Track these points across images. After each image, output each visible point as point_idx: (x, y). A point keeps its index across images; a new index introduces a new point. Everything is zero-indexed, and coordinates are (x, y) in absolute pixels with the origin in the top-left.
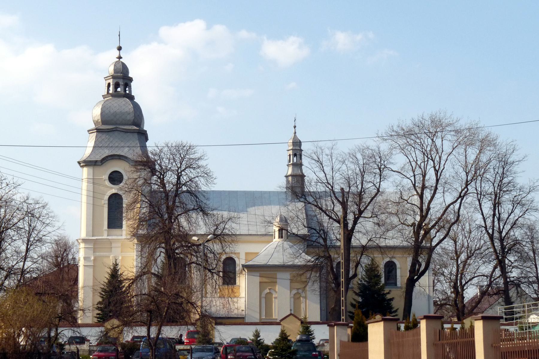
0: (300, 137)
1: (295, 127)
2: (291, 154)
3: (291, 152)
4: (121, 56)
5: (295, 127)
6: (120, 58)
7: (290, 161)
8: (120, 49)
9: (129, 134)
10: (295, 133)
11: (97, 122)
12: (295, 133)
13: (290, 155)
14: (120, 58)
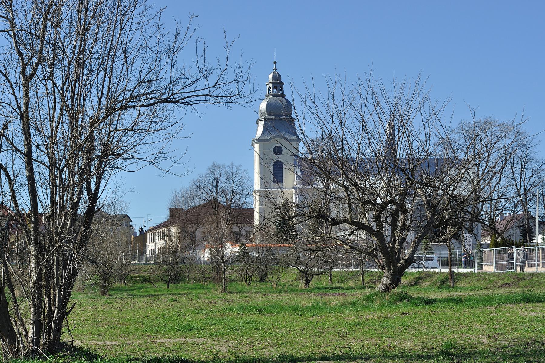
8: (275, 63)
11: (263, 111)
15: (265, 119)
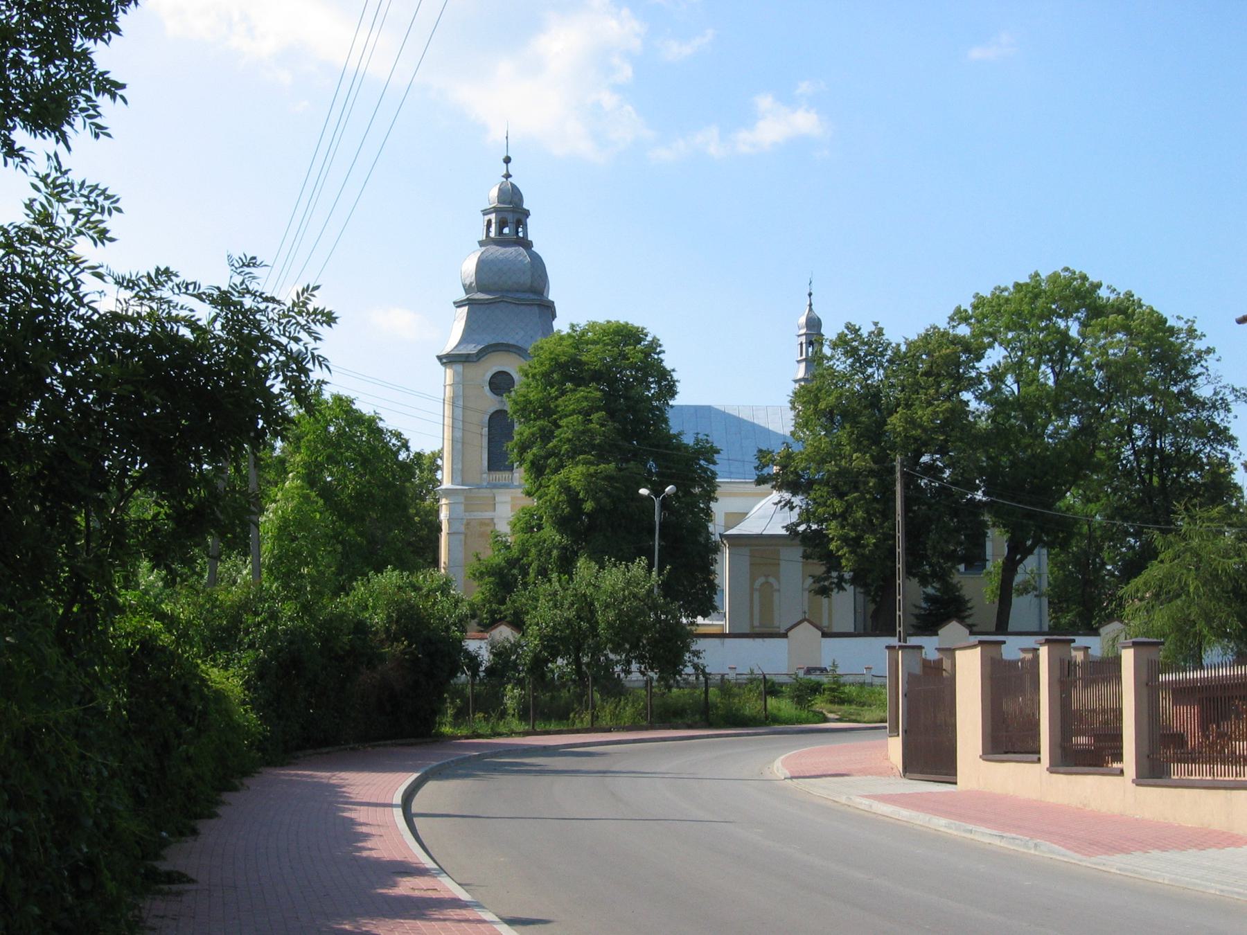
0: (818, 312)
1: (810, 295)
2: (804, 341)
3: (803, 339)
4: (511, 173)
5: (810, 295)
6: (508, 176)
7: (801, 355)
8: (507, 160)
9: (523, 307)
10: (811, 305)
12: (811, 305)
13: (801, 344)
14: (508, 176)
15: (469, 302)
